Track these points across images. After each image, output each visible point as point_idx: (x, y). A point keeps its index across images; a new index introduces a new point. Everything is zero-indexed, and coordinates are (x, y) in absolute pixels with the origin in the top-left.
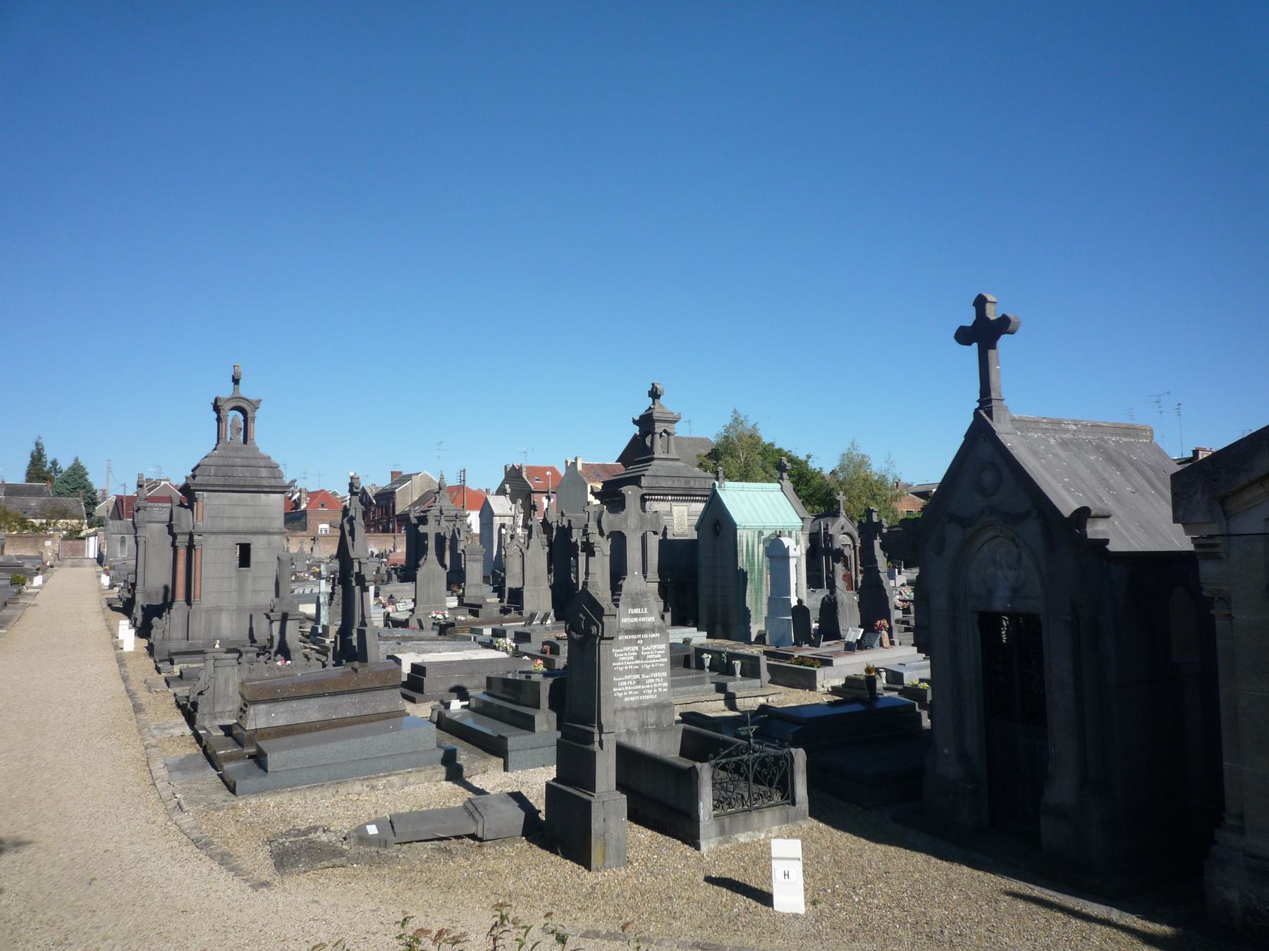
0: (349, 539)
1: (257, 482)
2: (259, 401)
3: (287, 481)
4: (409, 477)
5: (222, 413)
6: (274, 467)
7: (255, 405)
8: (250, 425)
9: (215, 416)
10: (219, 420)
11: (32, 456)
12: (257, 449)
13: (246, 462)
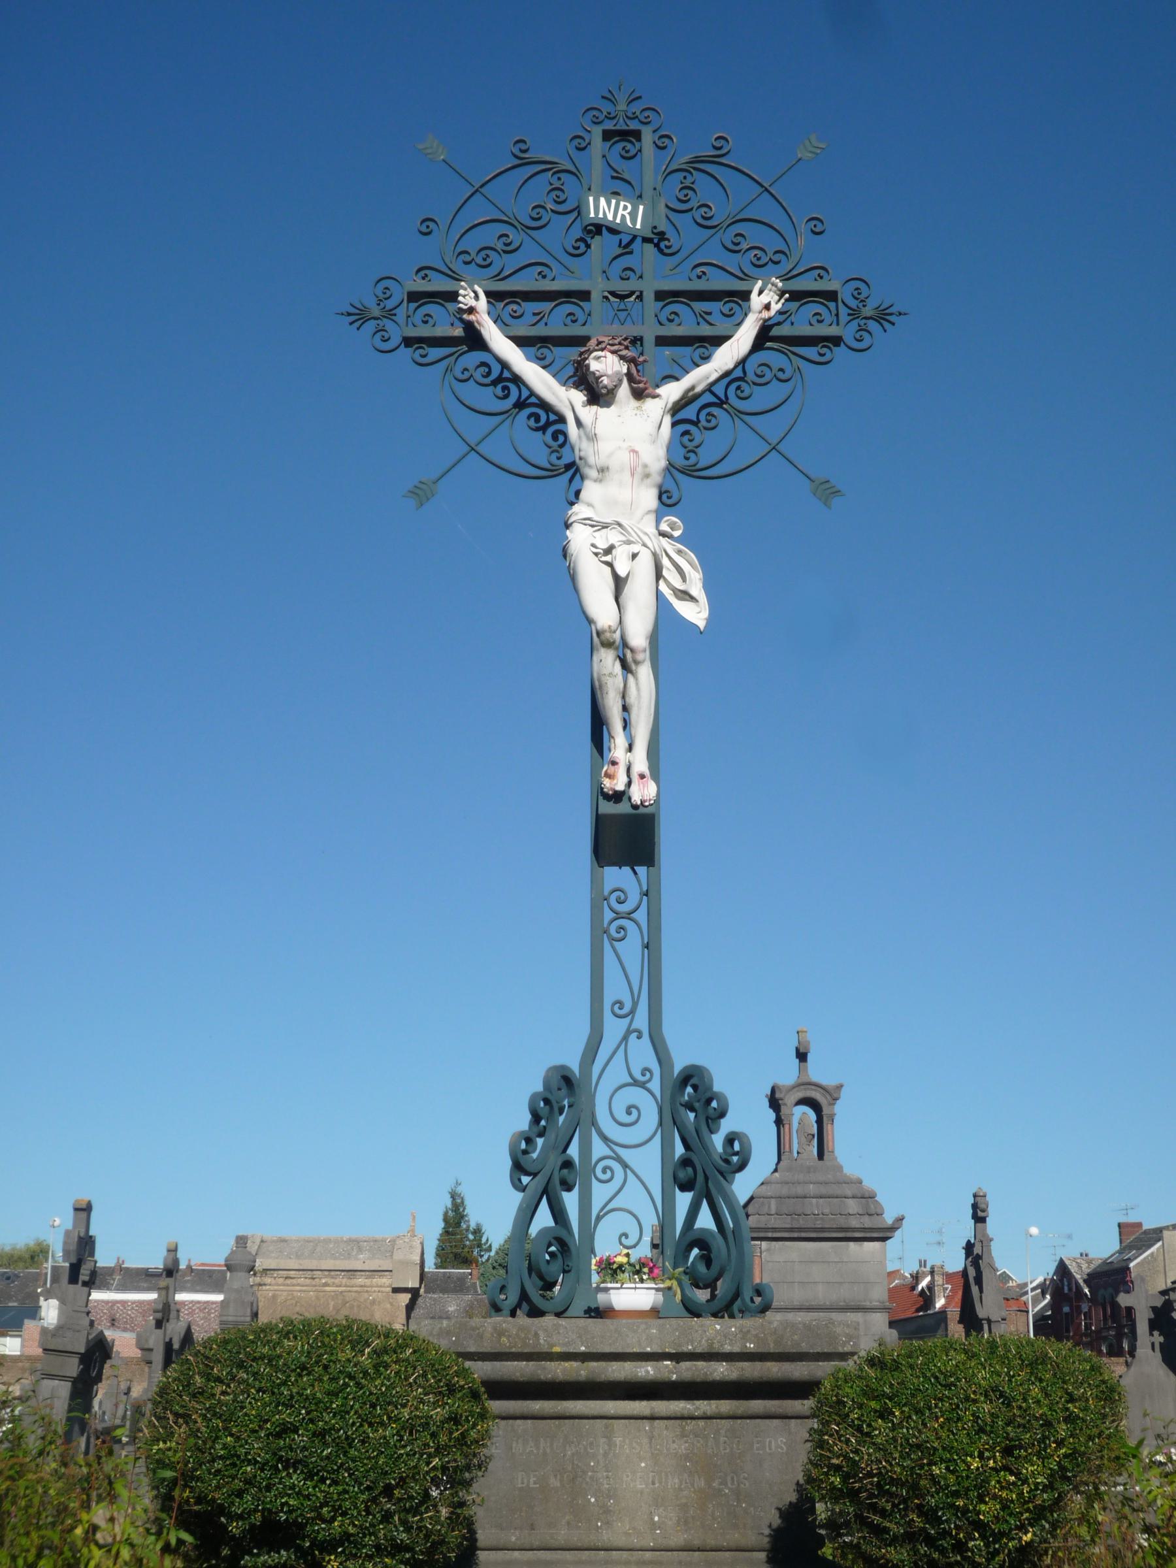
0: (975, 1289)
1: (842, 1222)
2: (830, 508)
3: (889, 1218)
4: (1156, 1235)
5: (784, 1111)
6: (868, 1197)
7: (833, 1094)
8: (827, 1127)
9: (773, 1116)
10: (779, 1122)
11: (446, 1219)
12: (840, 1168)
13: (823, 1190)
